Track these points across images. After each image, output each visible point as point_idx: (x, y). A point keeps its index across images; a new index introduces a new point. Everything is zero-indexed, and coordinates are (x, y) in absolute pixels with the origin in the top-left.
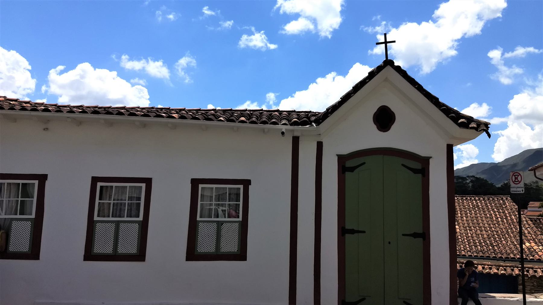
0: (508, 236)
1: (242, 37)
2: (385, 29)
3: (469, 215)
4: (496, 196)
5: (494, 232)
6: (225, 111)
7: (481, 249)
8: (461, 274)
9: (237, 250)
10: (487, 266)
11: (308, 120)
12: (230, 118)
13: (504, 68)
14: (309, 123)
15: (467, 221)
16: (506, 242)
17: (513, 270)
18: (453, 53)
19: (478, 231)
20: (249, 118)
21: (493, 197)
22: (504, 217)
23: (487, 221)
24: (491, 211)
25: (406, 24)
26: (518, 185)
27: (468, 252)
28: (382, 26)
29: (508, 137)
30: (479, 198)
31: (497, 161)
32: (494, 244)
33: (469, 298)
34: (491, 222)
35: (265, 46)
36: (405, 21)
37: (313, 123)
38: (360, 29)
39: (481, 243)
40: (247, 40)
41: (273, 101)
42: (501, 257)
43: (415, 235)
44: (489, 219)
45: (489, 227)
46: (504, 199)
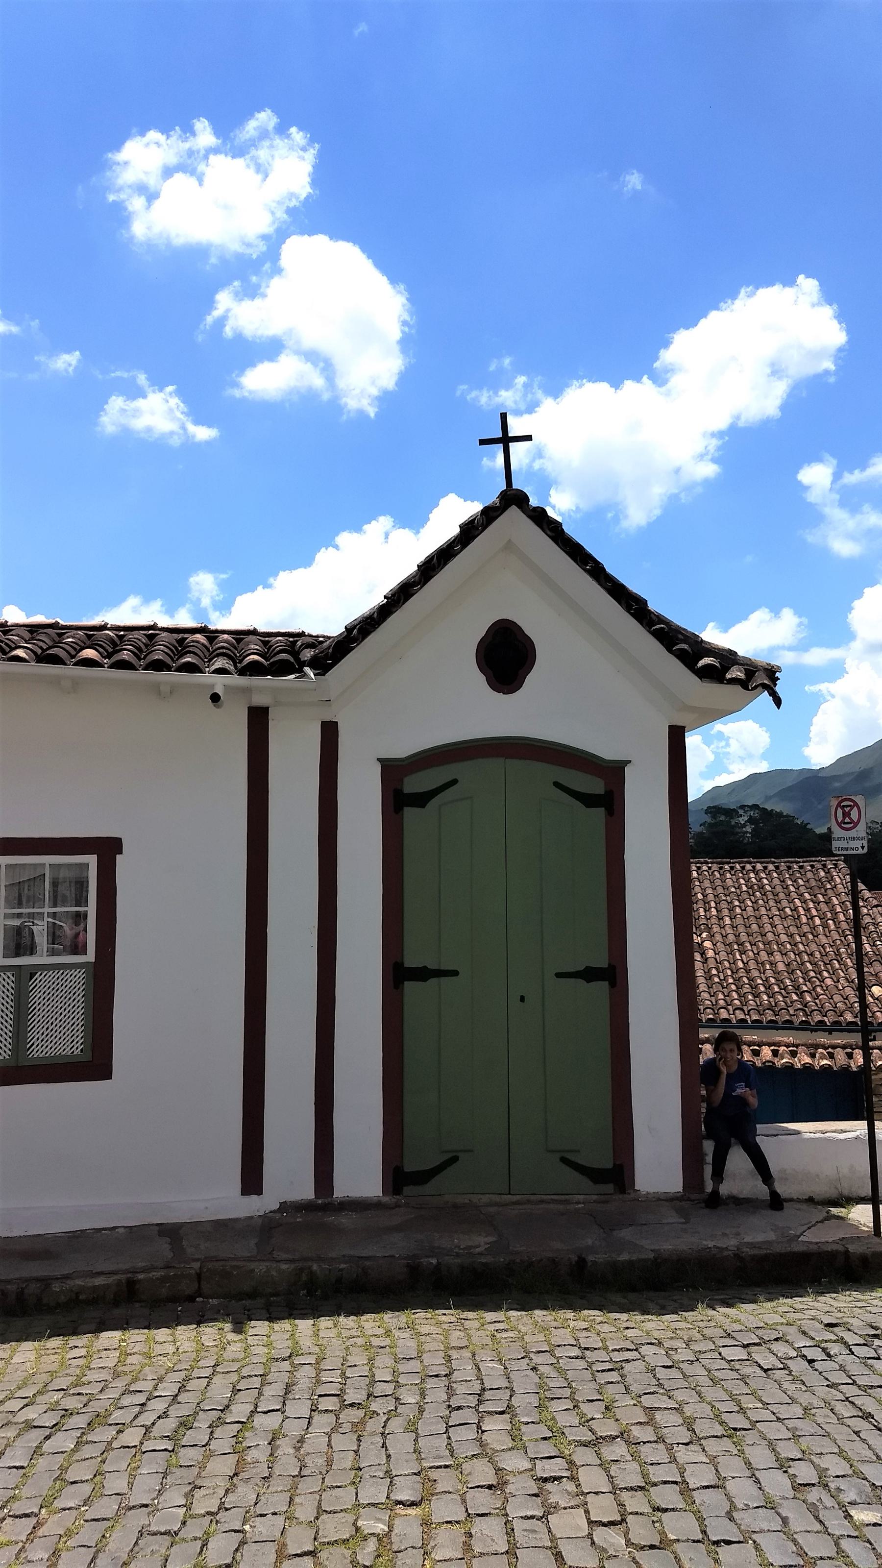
0: (840, 965)
1: (107, 403)
2: (525, 395)
3: (738, 910)
4: (808, 859)
5: (804, 954)
6: (34, 629)
7: (769, 1001)
8: (710, 1071)
9: (82, 1050)
10: (785, 1049)
11: (292, 660)
12: (50, 652)
13: (837, 514)
14: (293, 667)
15: (733, 927)
16: (835, 982)
17: (850, 1056)
18: (709, 470)
19: (763, 953)
20: (110, 650)
21: (800, 862)
22: (829, 915)
23: (785, 927)
24: (796, 900)
25: (581, 386)
26: (852, 833)
27: (737, 1012)
28: (517, 386)
29: (847, 701)
30: (765, 865)
31: (816, 765)
32: (804, 986)
33: (733, 1140)
34: (796, 929)
35: (181, 432)
36: (579, 378)
37: (307, 670)
38: (458, 393)
39: (768, 987)
40: (123, 411)
41: (212, 597)
42: (821, 1022)
43: (589, 974)
44: (789, 922)
45: (790, 943)
46: (829, 867)
